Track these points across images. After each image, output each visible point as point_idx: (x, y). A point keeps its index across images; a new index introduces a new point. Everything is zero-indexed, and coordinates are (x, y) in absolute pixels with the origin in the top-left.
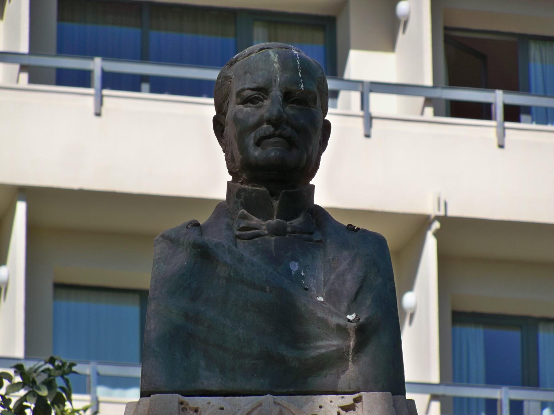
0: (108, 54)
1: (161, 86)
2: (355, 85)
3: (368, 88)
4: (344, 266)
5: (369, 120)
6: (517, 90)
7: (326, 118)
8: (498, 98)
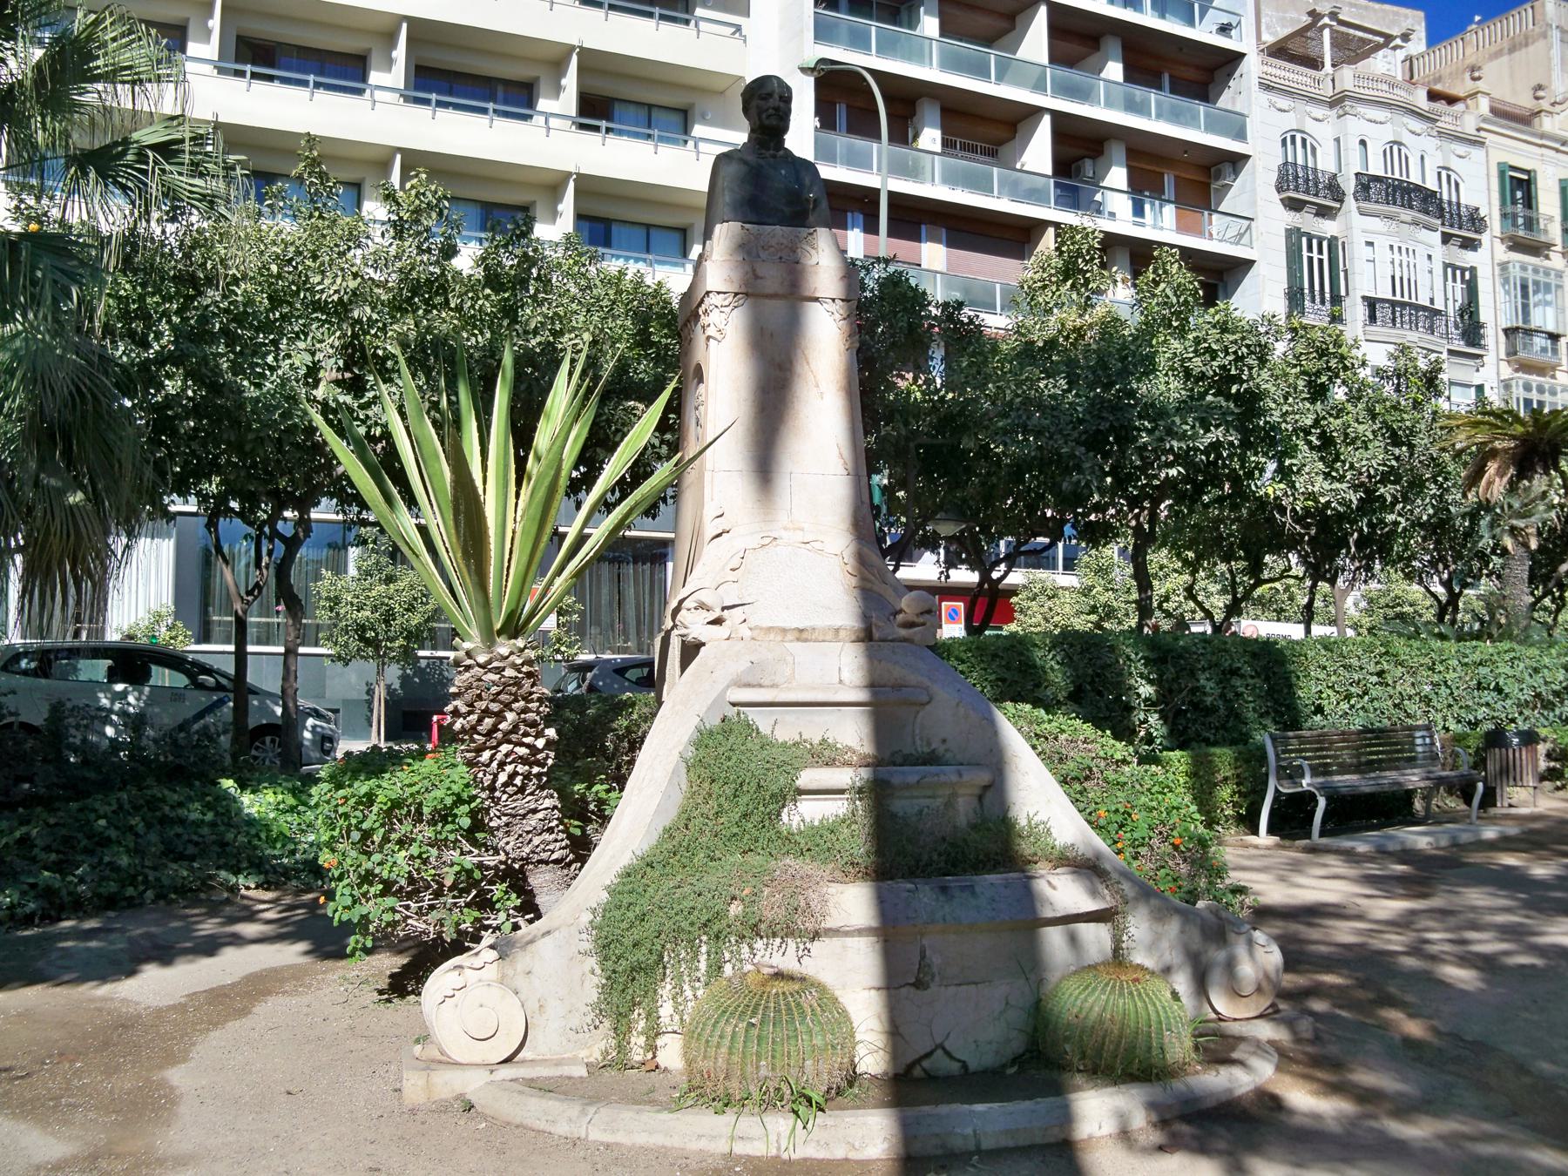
0: (439, 93)
1: (457, 107)
2: (542, 113)
3: (547, 116)
4: (548, 803)
5: (549, 129)
6: (916, 176)
7: (154, 668)
8: (603, 124)
